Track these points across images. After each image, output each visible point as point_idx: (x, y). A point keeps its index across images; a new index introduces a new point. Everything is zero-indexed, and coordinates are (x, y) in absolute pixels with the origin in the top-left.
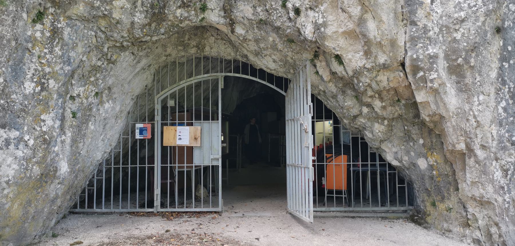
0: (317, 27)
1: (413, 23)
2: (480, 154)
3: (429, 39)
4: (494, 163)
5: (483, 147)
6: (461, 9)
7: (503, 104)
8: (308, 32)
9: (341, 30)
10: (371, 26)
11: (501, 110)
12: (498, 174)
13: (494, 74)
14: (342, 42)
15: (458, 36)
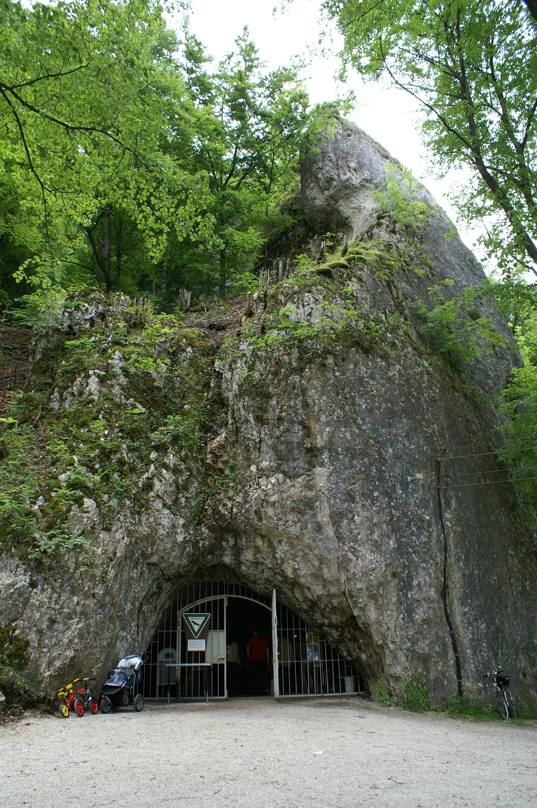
0: (295, 570)
1: (348, 571)
2: (391, 646)
3: (357, 579)
4: (400, 652)
5: (393, 642)
6: (372, 564)
7: (402, 616)
8: (289, 572)
9: (309, 573)
10: (325, 570)
11: (401, 620)
12: (403, 659)
13: (394, 599)
14: (310, 579)
15: (372, 578)
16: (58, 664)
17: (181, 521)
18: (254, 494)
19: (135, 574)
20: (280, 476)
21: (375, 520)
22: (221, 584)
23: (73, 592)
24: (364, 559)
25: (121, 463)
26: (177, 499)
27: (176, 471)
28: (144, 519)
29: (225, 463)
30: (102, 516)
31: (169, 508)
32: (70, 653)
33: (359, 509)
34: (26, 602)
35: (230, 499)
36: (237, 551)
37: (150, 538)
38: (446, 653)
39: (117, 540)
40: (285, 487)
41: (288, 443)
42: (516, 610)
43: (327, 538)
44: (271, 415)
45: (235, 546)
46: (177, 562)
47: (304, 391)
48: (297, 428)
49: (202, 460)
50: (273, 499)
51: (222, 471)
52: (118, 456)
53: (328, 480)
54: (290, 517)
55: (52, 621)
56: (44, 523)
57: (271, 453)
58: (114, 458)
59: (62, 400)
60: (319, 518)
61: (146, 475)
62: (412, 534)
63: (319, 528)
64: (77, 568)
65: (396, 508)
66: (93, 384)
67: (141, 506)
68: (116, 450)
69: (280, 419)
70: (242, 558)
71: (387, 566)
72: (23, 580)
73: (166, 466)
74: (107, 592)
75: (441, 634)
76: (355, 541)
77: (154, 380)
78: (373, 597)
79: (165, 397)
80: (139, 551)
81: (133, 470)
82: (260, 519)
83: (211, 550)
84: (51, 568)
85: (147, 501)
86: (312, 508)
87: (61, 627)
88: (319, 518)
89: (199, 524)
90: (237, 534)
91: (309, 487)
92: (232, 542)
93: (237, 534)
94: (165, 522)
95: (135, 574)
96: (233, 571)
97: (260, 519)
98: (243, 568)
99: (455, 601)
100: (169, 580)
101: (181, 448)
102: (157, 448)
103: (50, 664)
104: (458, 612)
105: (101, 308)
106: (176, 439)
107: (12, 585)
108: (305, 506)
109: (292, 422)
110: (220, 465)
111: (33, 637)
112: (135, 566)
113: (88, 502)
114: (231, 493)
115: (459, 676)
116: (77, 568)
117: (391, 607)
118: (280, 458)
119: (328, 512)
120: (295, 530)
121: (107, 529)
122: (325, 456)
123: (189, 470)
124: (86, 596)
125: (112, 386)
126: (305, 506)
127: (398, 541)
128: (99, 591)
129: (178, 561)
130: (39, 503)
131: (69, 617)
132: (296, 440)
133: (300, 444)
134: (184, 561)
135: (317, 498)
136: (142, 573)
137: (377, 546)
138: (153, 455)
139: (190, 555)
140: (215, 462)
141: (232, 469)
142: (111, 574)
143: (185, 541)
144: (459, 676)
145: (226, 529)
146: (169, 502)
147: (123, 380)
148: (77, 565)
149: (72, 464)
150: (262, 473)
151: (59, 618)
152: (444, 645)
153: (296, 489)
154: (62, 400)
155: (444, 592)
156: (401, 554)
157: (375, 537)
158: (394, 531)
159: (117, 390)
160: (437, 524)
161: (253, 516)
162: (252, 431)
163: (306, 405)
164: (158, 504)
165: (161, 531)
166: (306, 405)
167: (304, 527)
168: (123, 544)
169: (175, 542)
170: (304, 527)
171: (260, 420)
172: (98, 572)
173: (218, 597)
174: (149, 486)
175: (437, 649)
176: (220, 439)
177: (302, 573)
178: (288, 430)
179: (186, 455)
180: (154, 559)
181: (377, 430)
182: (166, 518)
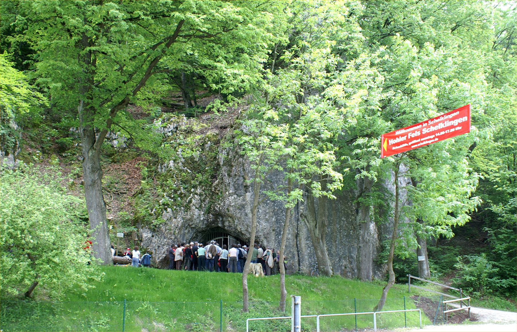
8: (239, 229)
16: (161, 258)
17: (202, 213)
18: (227, 202)
19: (186, 231)
20: (236, 196)
21: (267, 211)
22: (221, 233)
23: (165, 238)
24: (262, 225)
25: (181, 194)
26: (201, 205)
27: (200, 195)
28: (189, 213)
29: (219, 190)
30: (174, 214)
31: (198, 209)
32: (164, 255)
33: (261, 207)
34: (151, 242)
35: (219, 204)
36: (223, 222)
37: (191, 220)
38: (294, 257)
39: (179, 221)
40: (237, 200)
41: (238, 184)
42: (342, 242)
43: (249, 218)
44: (232, 174)
45: (222, 220)
46: (202, 227)
47: (243, 164)
48: (241, 178)
49: (211, 190)
50: (232, 204)
51: (218, 194)
52: (180, 191)
53: (251, 197)
54: (237, 211)
55: (159, 247)
56: (155, 217)
57: (233, 187)
58: (179, 192)
59: (162, 169)
60: (246, 211)
61: (190, 198)
62: (283, 215)
63: (246, 215)
64: (166, 231)
65: (277, 206)
66: (171, 163)
67: (187, 208)
68: (179, 189)
69: (235, 175)
70: (225, 224)
71: (270, 227)
72: (150, 235)
73: (196, 194)
74: (175, 238)
75: (292, 250)
76: (259, 219)
77: (194, 158)
78: (265, 238)
79: (198, 165)
80: (187, 224)
81: (185, 196)
82: (229, 211)
83: (213, 222)
84: (158, 231)
85: (190, 207)
86: (244, 208)
87: (161, 248)
88: (246, 211)
89: (209, 213)
90: (222, 217)
91: (244, 200)
92: (221, 219)
93: (222, 217)
94: (196, 213)
95: (186, 231)
96: (223, 228)
97: (229, 211)
98: (226, 228)
99: (303, 239)
100: (200, 232)
101: (203, 186)
102: (194, 187)
103: (158, 258)
104: (303, 243)
105: (175, 125)
106: (201, 183)
107: (147, 237)
108: (242, 207)
109: (240, 176)
110: (217, 192)
111: (153, 251)
112: (186, 229)
113: (169, 210)
114: (220, 202)
115: (299, 265)
116: (166, 231)
117: (272, 241)
118: (236, 189)
119: (250, 209)
120: (239, 215)
121: (176, 218)
122: (250, 188)
123: (205, 194)
124: (169, 239)
125: (179, 163)
126: (242, 207)
127: (276, 218)
128: (173, 237)
129: (202, 226)
130: (154, 211)
131: (164, 245)
132: (240, 183)
133: (242, 184)
134: (204, 226)
135: (246, 204)
136: (189, 231)
137: (267, 220)
138: (192, 190)
139: (206, 224)
140: (215, 190)
141: (221, 193)
142: (177, 232)
143: (204, 220)
144: (299, 265)
145: (218, 215)
146: (198, 207)
147: (183, 160)
148: (166, 230)
149: (163, 197)
150: (230, 195)
151: (161, 246)
152: (293, 255)
153: (240, 201)
154: (162, 169)
155: (297, 236)
156: (277, 223)
157: (267, 217)
158: (275, 215)
159: (180, 164)
160: (295, 211)
161: (226, 210)
162: (227, 180)
163: (244, 170)
164: (194, 208)
165: (195, 217)
166: (244, 170)
167: (241, 214)
168: (181, 222)
169: (200, 220)
170: (241, 214)
171: (229, 175)
172: (172, 232)
173: (220, 238)
174: (190, 202)
175: (290, 255)
176: (217, 182)
177: (242, 230)
178: (238, 179)
179: (205, 189)
180: (193, 226)
181: (271, 177)
182: (196, 212)
